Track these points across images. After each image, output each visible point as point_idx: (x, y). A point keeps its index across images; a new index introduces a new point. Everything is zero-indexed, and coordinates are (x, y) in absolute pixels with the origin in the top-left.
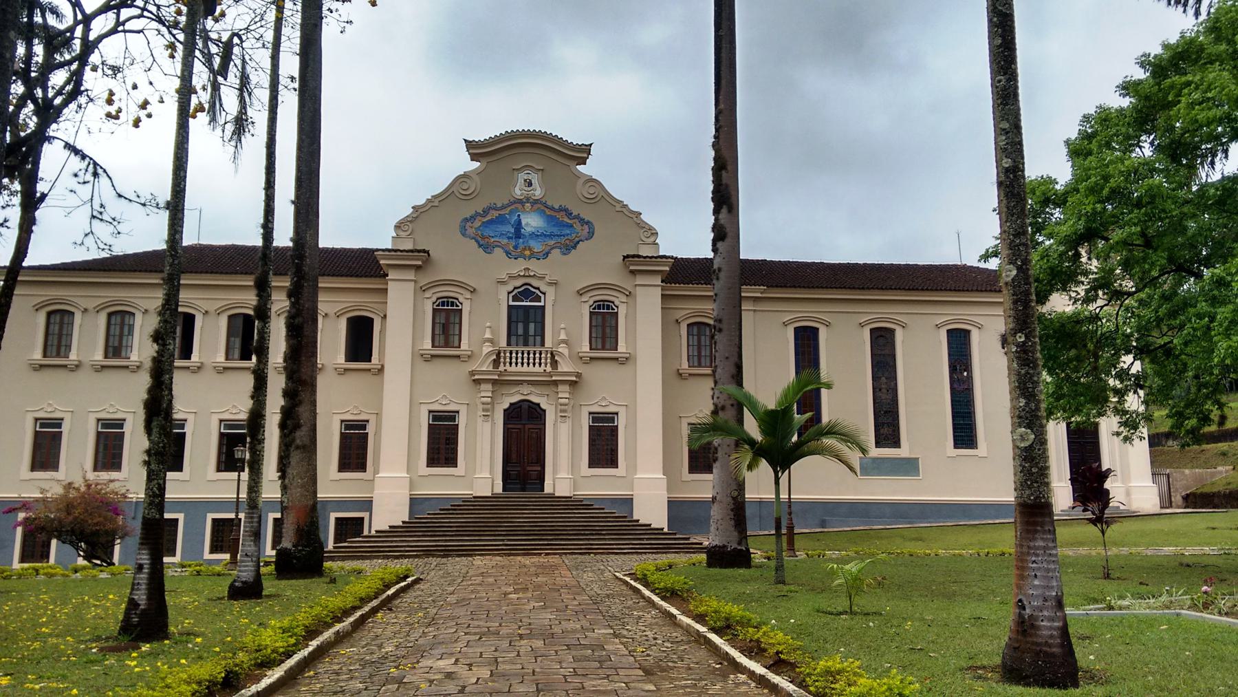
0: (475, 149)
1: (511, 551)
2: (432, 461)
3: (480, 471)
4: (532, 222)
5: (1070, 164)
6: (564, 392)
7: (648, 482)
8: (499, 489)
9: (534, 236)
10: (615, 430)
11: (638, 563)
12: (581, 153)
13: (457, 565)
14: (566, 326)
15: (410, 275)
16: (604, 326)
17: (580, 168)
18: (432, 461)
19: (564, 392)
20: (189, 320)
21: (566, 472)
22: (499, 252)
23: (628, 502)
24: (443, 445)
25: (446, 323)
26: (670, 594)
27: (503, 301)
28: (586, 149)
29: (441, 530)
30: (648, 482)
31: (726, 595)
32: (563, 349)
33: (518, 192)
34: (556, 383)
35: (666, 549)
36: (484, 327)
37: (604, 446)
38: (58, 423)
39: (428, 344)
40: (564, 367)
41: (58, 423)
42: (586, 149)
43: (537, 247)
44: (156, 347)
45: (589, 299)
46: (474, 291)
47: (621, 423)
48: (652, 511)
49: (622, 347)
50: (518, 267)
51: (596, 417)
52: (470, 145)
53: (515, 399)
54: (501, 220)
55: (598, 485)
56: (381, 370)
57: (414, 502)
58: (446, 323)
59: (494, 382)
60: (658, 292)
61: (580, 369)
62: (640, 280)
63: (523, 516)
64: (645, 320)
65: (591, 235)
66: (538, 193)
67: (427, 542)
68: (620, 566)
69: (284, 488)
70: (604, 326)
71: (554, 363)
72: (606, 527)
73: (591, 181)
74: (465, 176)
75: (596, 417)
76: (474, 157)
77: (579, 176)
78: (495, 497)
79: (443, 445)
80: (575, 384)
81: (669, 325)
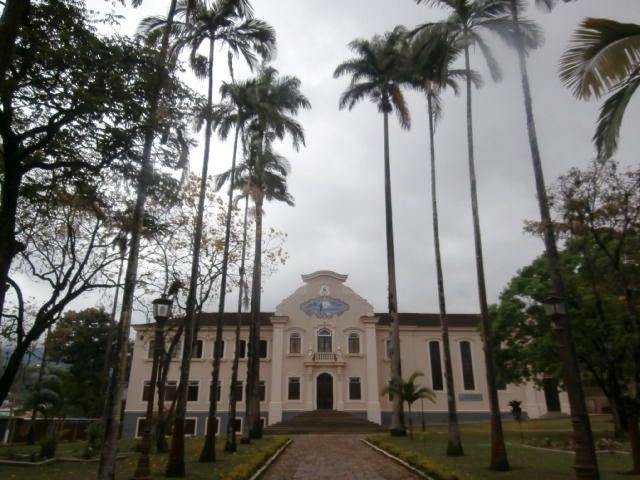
0: (306, 278)
1: (322, 432)
2: (352, 397)
3: (308, 402)
4: (326, 304)
5: (517, 275)
6: (339, 370)
7: (373, 406)
8: (316, 408)
9: (327, 309)
10: (298, 384)
11: (371, 436)
12: (344, 278)
13: (303, 437)
14: (340, 344)
15: (282, 326)
16: (354, 343)
17: (344, 284)
18: (352, 397)
19: (339, 370)
20: (201, 343)
21: (341, 401)
22: (314, 316)
23: (365, 413)
24: (294, 391)
25: (295, 344)
26: (377, 444)
27: (316, 334)
28: (346, 277)
29: (295, 423)
30: (373, 406)
31: (398, 445)
32: (339, 353)
33: (321, 293)
34: (337, 366)
35: (380, 431)
36: (309, 346)
37: (355, 390)
38: (358, 379)
39: (288, 352)
40: (339, 360)
41: (358, 379)
42: (346, 277)
43: (328, 314)
44: (261, 339)
45: (348, 333)
46: (305, 331)
47: (362, 382)
48: (375, 417)
49: (361, 352)
50: (321, 322)
51: (352, 380)
52: (303, 276)
53: (321, 372)
54: (315, 304)
55: (354, 406)
56: (270, 361)
57: (285, 414)
58: (295, 344)
59: (314, 366)
60: (374, 330)
61: (346, 361)
62: (368, 325)
63: (325, 419)
64: (370, 340)
65: (348, 309)
66: (328, 293)
67: (291, 429)
68: (362, 437)
69: (247, 408)
70: (354, 343)
71: (336, 359)
72: (357, 423)
73: (348, 288)
74: (301, 288)
75: (352, 380)
76: (305, 281)
77: (343, 286)
78: (314, 411)
79: (294, 391)
80: (344, 367)
81: (379, 342)
